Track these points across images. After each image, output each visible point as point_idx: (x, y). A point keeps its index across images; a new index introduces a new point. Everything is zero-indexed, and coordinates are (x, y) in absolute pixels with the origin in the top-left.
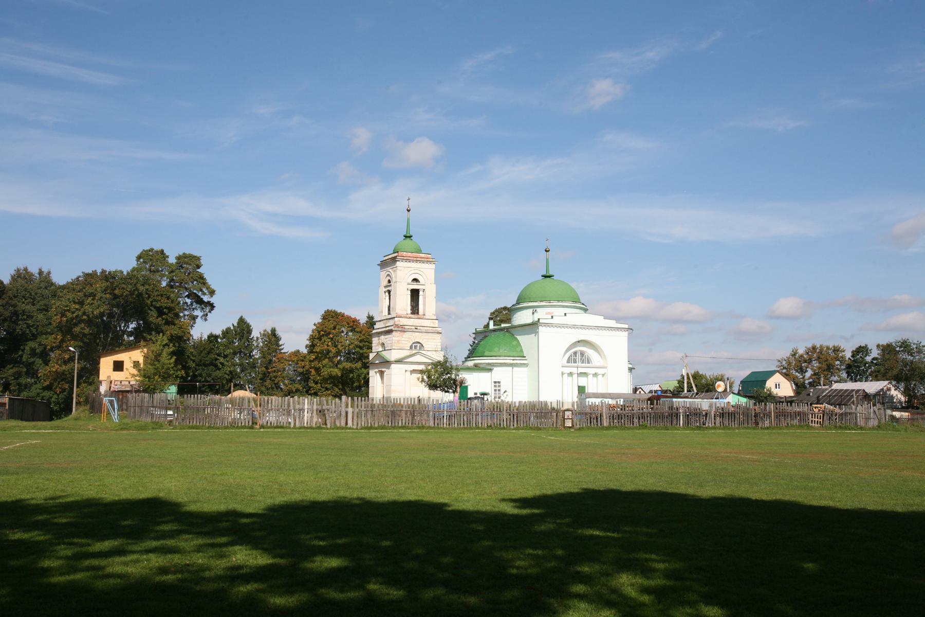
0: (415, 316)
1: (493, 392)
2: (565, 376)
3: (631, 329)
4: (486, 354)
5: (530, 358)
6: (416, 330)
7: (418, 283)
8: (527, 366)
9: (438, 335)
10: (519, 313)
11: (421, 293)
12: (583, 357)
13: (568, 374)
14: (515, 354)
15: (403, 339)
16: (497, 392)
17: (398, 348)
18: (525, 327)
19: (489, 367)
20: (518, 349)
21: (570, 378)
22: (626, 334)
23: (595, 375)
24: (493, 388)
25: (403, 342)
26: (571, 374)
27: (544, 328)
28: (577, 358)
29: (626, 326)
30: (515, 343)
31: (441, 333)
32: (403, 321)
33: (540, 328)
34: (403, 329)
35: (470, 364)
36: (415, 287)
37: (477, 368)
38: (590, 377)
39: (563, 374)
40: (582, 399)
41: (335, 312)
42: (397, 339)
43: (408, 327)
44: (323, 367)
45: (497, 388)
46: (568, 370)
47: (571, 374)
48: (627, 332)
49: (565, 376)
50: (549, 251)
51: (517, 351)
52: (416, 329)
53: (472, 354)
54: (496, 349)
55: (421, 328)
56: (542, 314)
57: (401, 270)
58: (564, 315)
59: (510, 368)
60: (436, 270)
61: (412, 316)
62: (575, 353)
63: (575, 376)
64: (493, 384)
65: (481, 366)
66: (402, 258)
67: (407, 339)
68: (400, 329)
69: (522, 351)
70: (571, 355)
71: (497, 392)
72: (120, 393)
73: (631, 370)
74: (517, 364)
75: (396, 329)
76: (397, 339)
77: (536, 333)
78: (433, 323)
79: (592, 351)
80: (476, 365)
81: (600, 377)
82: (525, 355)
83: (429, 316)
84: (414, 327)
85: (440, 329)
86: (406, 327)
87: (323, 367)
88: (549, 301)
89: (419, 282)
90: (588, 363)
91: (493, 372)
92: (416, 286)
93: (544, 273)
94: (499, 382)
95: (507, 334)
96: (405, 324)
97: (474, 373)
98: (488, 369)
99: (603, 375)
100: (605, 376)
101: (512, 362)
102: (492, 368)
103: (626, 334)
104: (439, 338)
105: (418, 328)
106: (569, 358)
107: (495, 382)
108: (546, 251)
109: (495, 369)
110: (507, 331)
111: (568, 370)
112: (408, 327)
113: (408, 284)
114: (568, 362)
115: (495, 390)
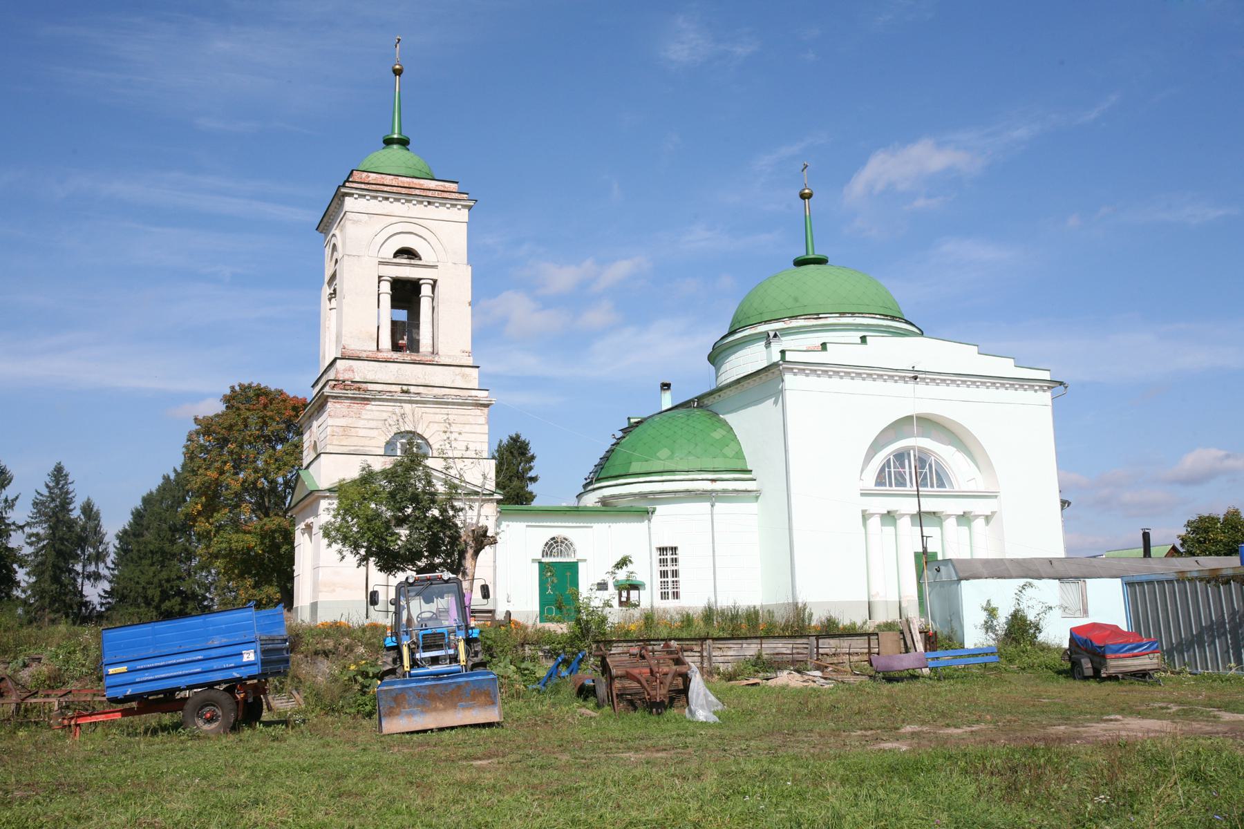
0: (407, 356)
1: (657, 579)
2: (875, 522)
3: (1061, 383)
4: (635, 467)
5: (765, 476)
6: (405, 397)
7: (413, 262)
8: (757, 498)
9: (478, 412)
10: (733, 357)
11: (426, 290)
12: (923, 467)
13: (882, 516)
14: (719, 463)
15: (361, 423)
16: (670, 579)
17: (345, 450)
18: (744, 383)
19: (643, 505)
20: (729, 451)
21: (889, 530)
22: (1046, 397)
23: (964, 518)
24: (657, 568)
25: (362, 432)
26: (890, 517)
27: (801, 378)
28: (907, 470)
29: (1046, 375)
30: (718, 434)
31: (487, 406)
32: (362, 371)
33: (788, 377)
34: (360, 394)
35: (591, 500)
36: (407, 271)
37: (609, 509)
38: (950, 523)
39: (865, 516)
40: (942, 584)
41: (261, 392)
42: (342, 422)
43: (379, 387)
44: (217, 532)
45: (670, 568)
46: (880, 505)
47: (890, 517)
48: (1048, 394)
49: (875, 522)
50: (810, 196)
51: (725, 456)
52: (406, 393)
53: (602, 472)
54: (664, 453)
55: (421, 390)
56: (798, 346)
57: (355, 222)
58: (859, 341)
59: (714, 516)
60: (470, 224)
61: (396, 355)
62: (900, 456)
63: (905, 523)
64: (656, 556)
65: (623, 503)
66: (363, 186)
67: (373, 424)
68: (350, 393)
69: (740, 455)
70: (889, 461)
71: (670, 579)
72: (744, 630)
73: (1065, 503)
74: (725, 491)
75: (337, 391)
76: (342, 422)
77: (778, 394)
78: (463, 375)
79: (951, 449)
80: (604, 501)
81: (979, 524)
82: (749, 468)
83: (449, 357)
84: (398, 388)
85: (485, 394)
86: (371, 387)
87: (217, 532)
88: (817, 316)
89: (420, 259)
90: (941, 484)
91: (654, 518)
92: (408, 268)
93: (801, 253)
94: (674, 549)
95: (698, 412)
96: (370, 377)
97: (596, 526)
98: (640, 510)
99: (988, 519)
100: (992, 522)
101: (708, 486)
102: (649, 507)
103: (1046, 397)
104: (482, 420)
105: (412, 389)
106: (882, 470)
107: (662, 550)
108: (803, 196)
109: (661, 509)
110: (699, 406)
111: (880, 505)
112: (379, 387)
113: (381, 263)
114: (880, 481)
115: (664, 574)
